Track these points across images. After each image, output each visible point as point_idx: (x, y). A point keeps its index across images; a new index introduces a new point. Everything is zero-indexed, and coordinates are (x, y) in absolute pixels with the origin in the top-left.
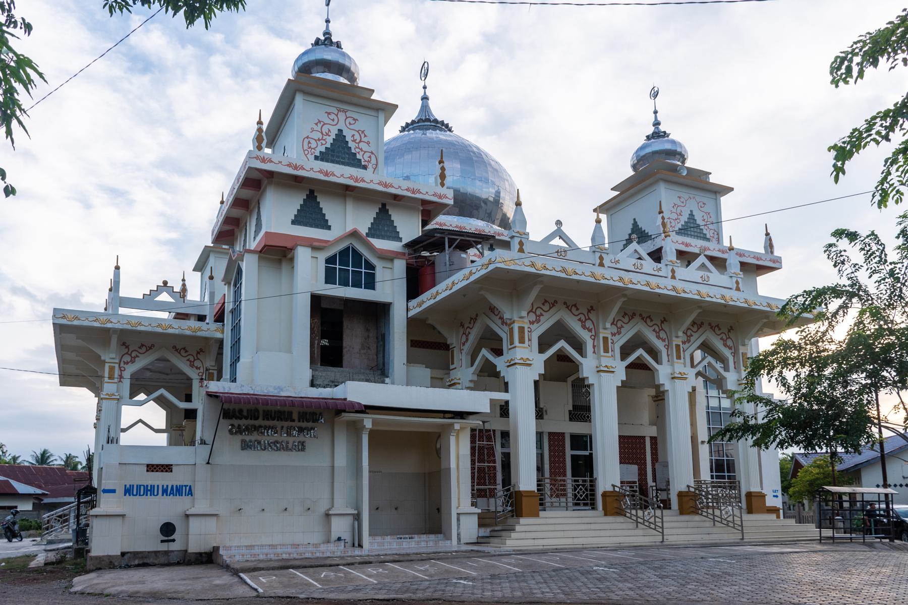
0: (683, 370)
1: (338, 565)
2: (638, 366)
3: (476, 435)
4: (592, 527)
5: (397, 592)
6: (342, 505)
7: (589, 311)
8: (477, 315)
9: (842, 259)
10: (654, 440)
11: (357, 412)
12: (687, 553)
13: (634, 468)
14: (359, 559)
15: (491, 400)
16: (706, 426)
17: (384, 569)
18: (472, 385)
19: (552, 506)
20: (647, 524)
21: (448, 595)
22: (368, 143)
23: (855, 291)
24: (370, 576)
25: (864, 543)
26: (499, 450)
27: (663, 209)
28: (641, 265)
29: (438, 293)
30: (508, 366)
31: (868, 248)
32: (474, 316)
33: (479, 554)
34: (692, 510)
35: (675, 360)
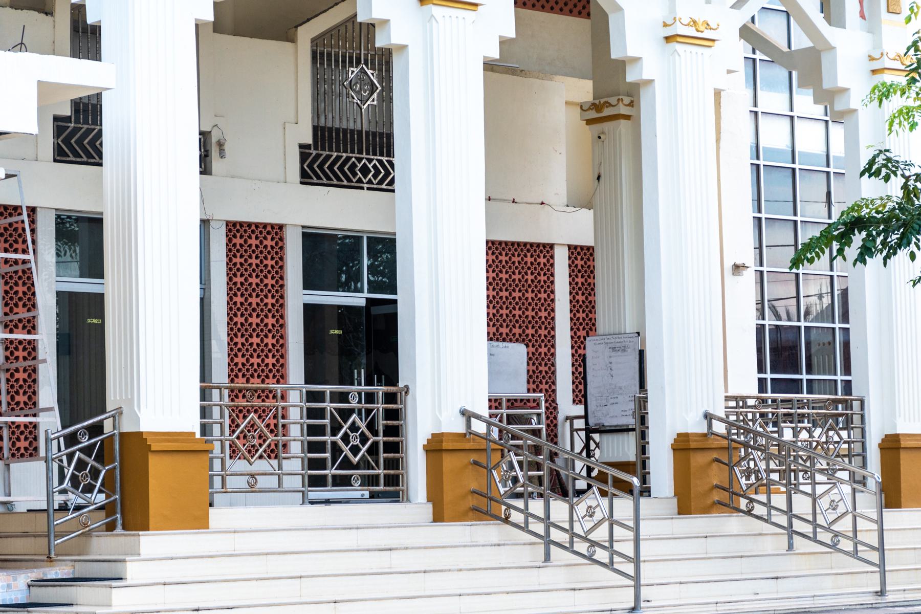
4: (398, 560)
13: (517, 353)
15: (44, 89)
16: (749, 213)
19: (252, 488)
20: (581, 547)
26: (49, 279)
34: (717, 496)
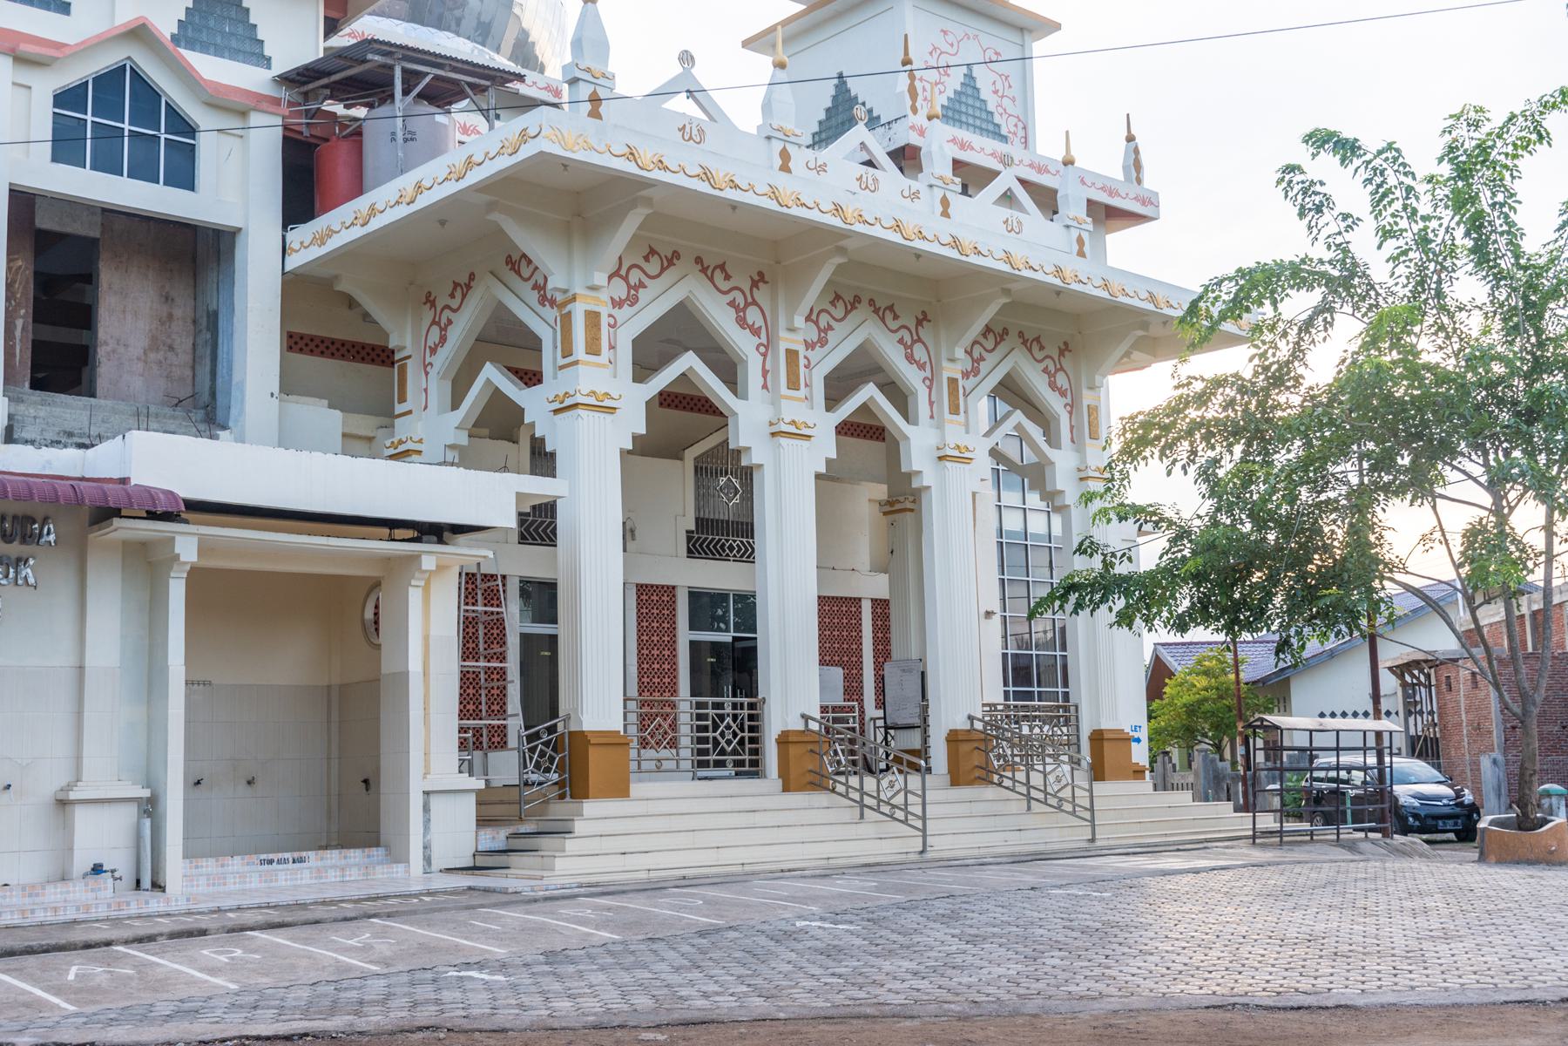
0: (964, 441)
1: (108, 944)
2: (862, 429)
3: (479, 588)
4: (758, 819)
5: (306, 1013)
6: (106, 773)
7: (755, 284)
8: (472, 277)
9: (1317, 199)
10: (881, 607)
11: (152, 516)
12: (991, 876)
14: (166, 925)
17: (246, 950)
18: (450, 456)
19: (659, 769)
20: (886, 809)
21: (455, 1015)
22: (1013, 100)
23: (1345, 281)
24: (213, 971)
25: (1338, 842)
27: (912, 55)
28: (875, 180)
29: (373, 211)
30: (556, 411)
31: (1378, 180)
32: (464, 279)
33: (494, 898)
34: (978, 773)
35: (947, 416)
